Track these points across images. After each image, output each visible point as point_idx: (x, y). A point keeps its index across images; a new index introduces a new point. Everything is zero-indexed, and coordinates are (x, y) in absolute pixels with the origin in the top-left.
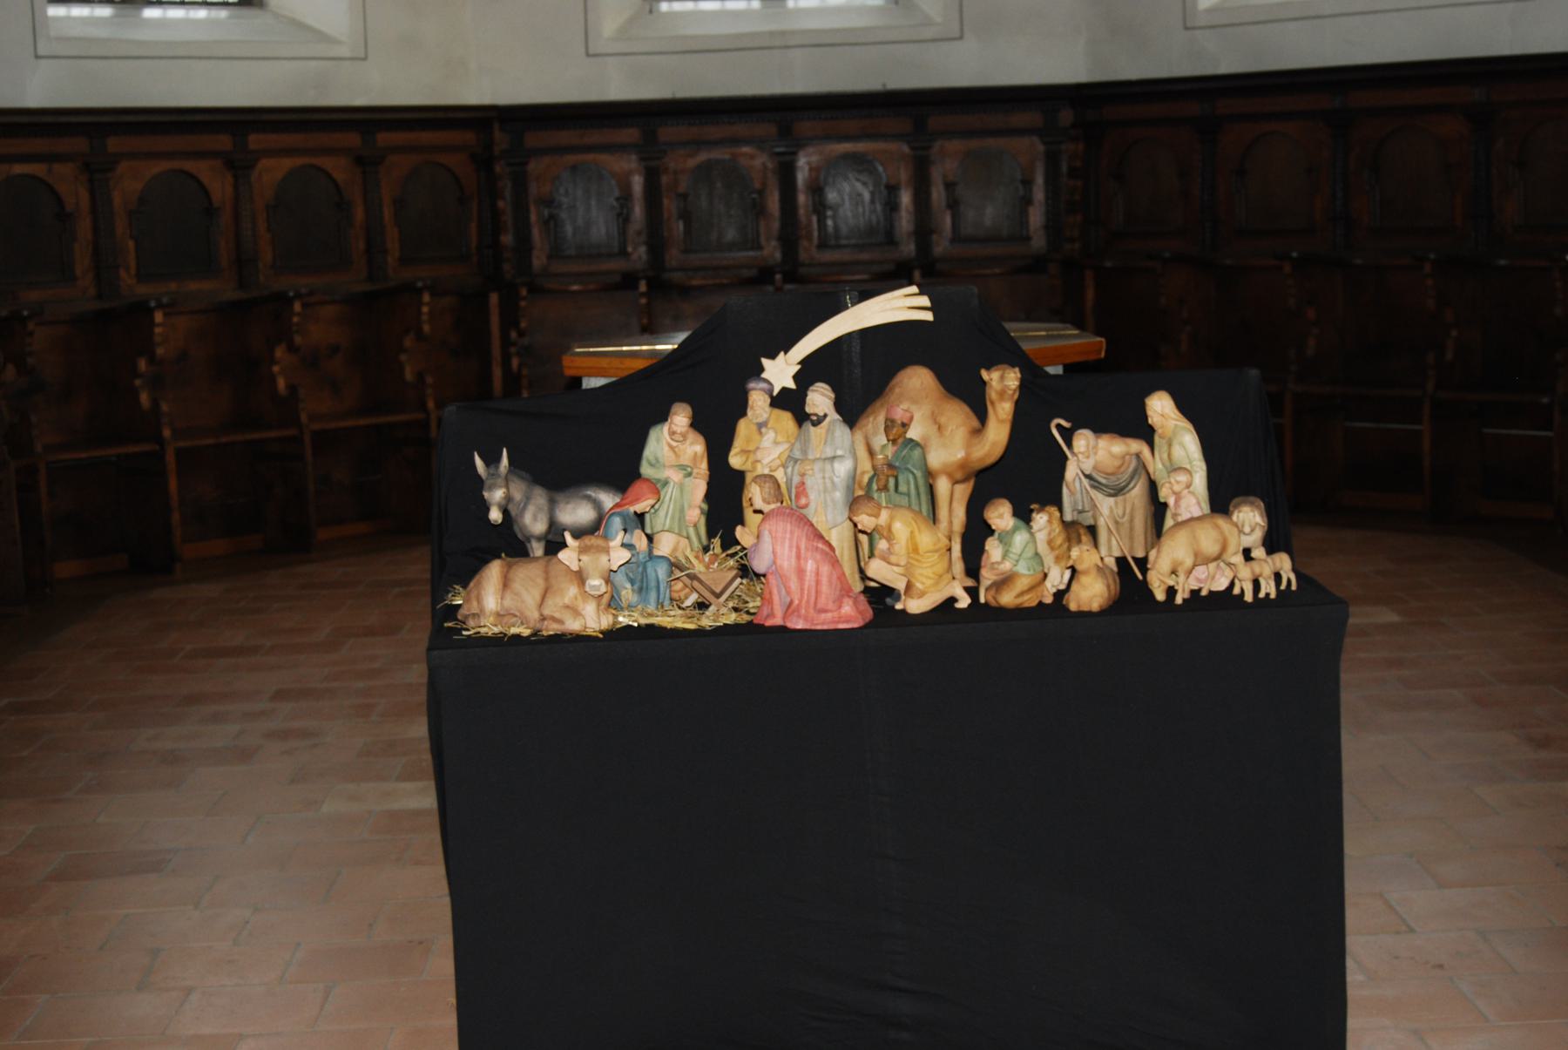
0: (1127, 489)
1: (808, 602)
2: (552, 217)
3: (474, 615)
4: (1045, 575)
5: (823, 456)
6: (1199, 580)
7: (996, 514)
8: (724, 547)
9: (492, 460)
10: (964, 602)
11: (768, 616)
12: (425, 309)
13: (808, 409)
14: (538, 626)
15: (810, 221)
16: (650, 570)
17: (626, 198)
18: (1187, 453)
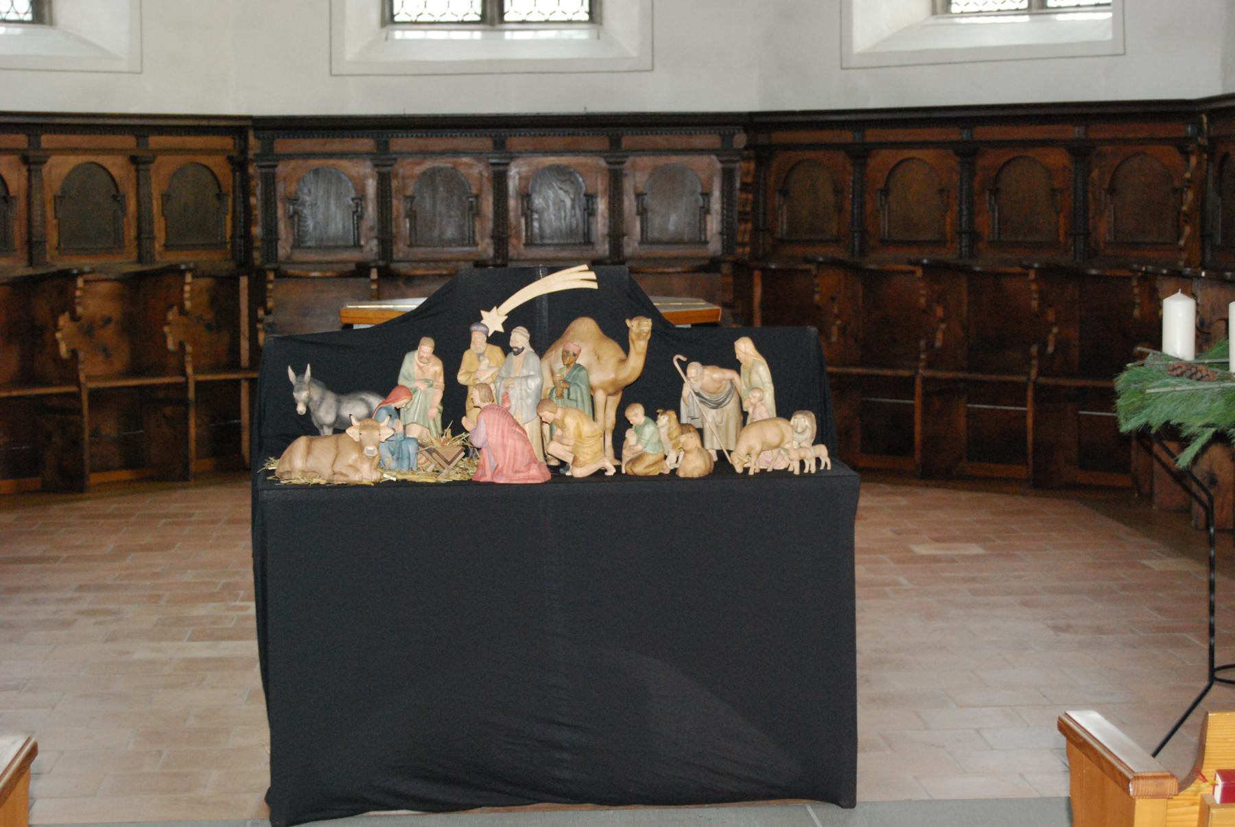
0: (724, 404)
1: (508, 466)
2: (296, 212)
3: (289, 472)
4: (665, 457)
5: (521, 375)
6: (767, 462)
7: (633, 413)
8: (453, 435)
9: (300, 372)
11: (481, 476)
12: (187, 288)
13: (512, 344)
14: (331, 479)
15: (519, 223)
16: (404, 447)
17: (360, 198)
18: (761, 378)
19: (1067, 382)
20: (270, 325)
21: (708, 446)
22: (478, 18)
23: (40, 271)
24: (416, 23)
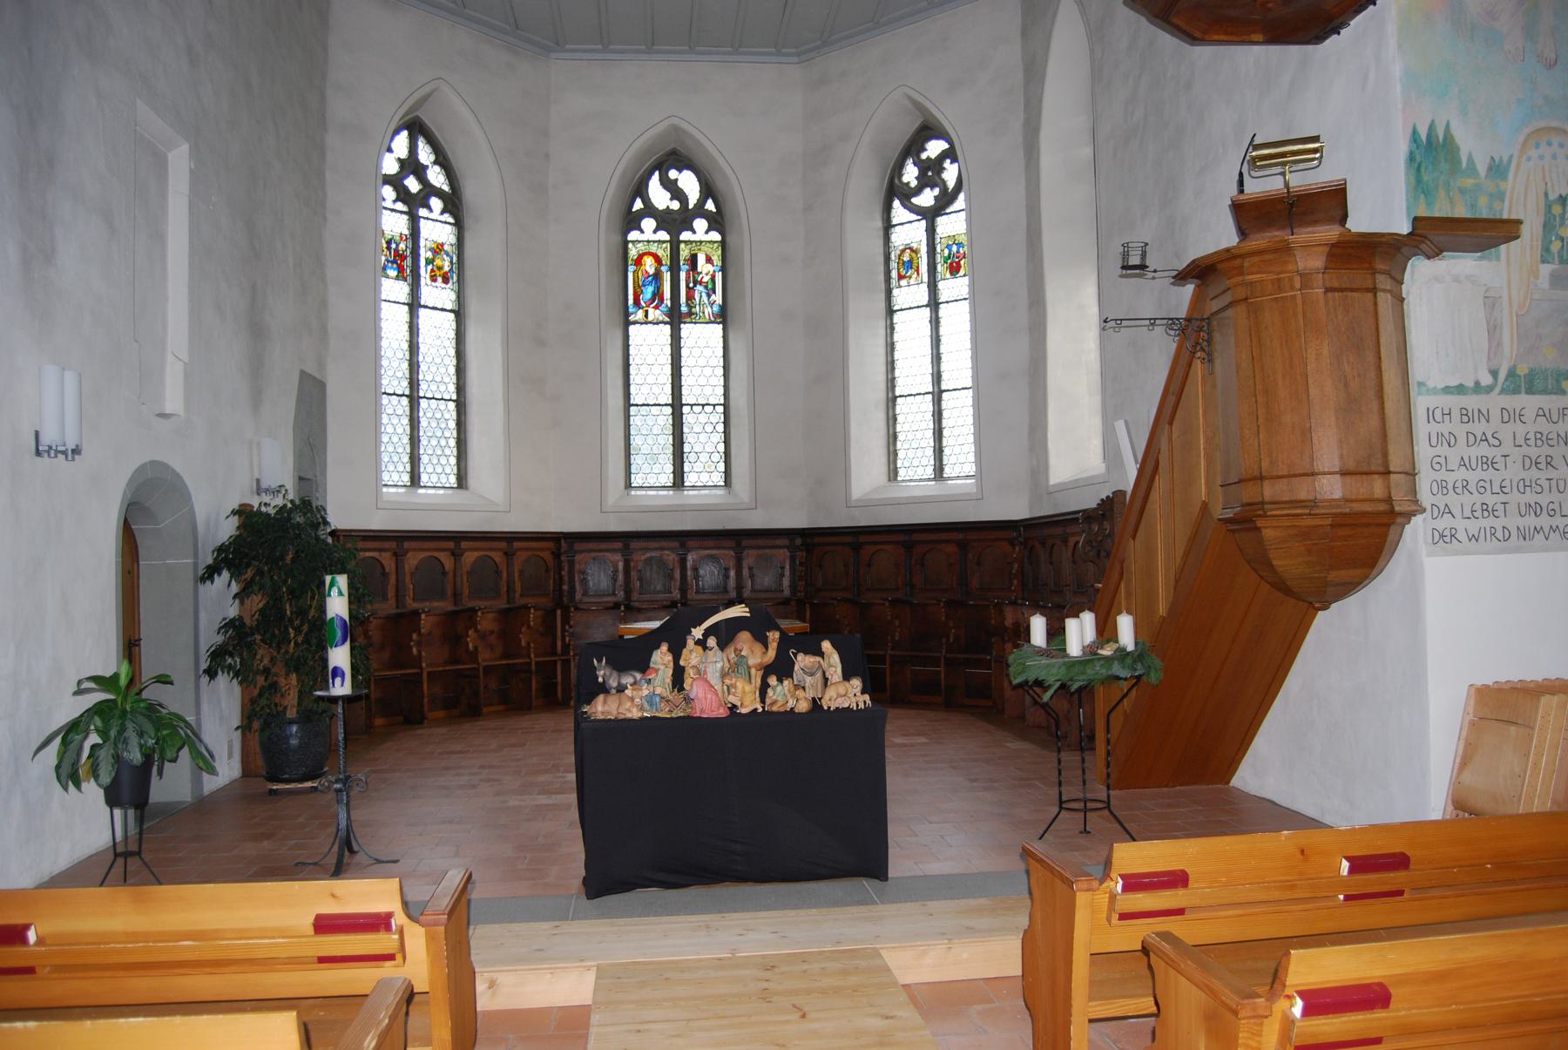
2: (584, 578)
3: (595, 713)
8: (679, 692)
9: (600, 661)
10: (760, 710)
12: (532, 616)
16: (654, 699)
17: (616, 571)
19: (959, 656)
20: (572, 633)
22: (671, 485)
23: (460, 608)
24: (642, 487)
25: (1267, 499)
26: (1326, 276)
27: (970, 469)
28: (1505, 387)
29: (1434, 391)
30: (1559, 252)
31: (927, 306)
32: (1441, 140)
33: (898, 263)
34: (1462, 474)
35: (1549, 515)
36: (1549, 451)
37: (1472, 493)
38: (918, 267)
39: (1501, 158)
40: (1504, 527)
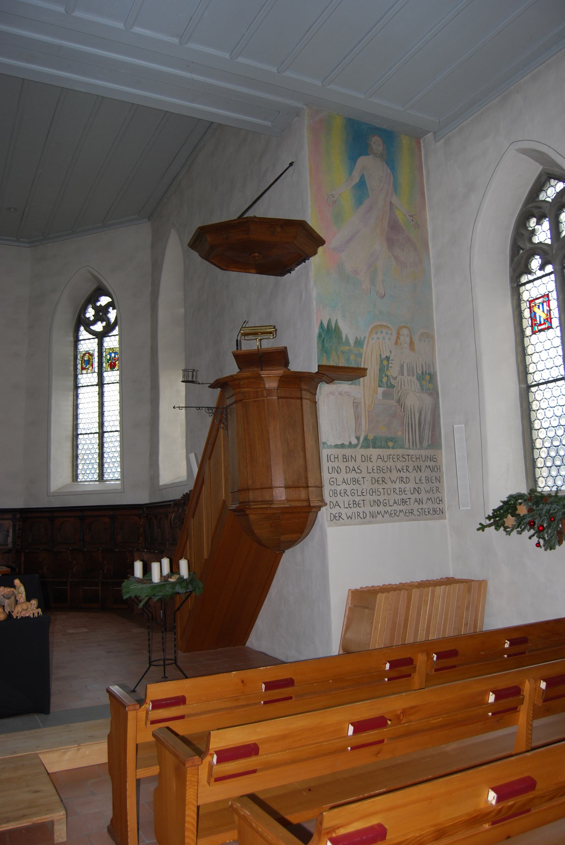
21: (6, 610)
25: (251, 500)
26: (279, 391)
27: (117, 476)
28: (363, 445)
29: (330, 447)
30: (386, 382)
31: (96, 385)
32: (333, 328)
33: (82, 361)
34: (344, 486)
35: (384, 505)
36: (383, 475)
37: (348, 496)
38: (92, 364)
39: (360, 338)
40: (363, 512)
